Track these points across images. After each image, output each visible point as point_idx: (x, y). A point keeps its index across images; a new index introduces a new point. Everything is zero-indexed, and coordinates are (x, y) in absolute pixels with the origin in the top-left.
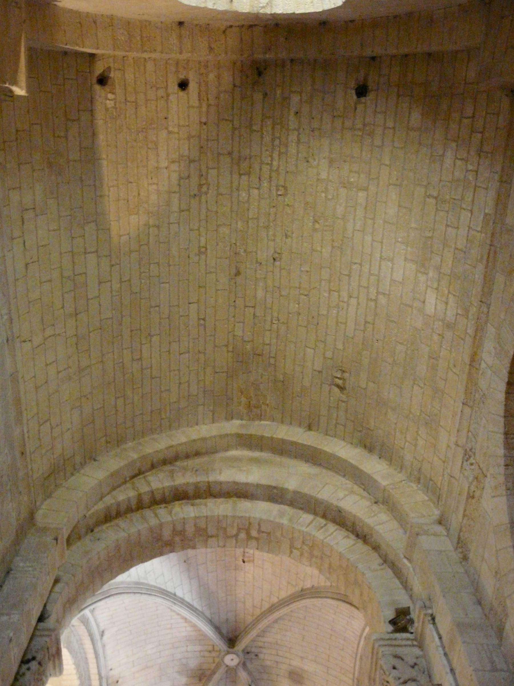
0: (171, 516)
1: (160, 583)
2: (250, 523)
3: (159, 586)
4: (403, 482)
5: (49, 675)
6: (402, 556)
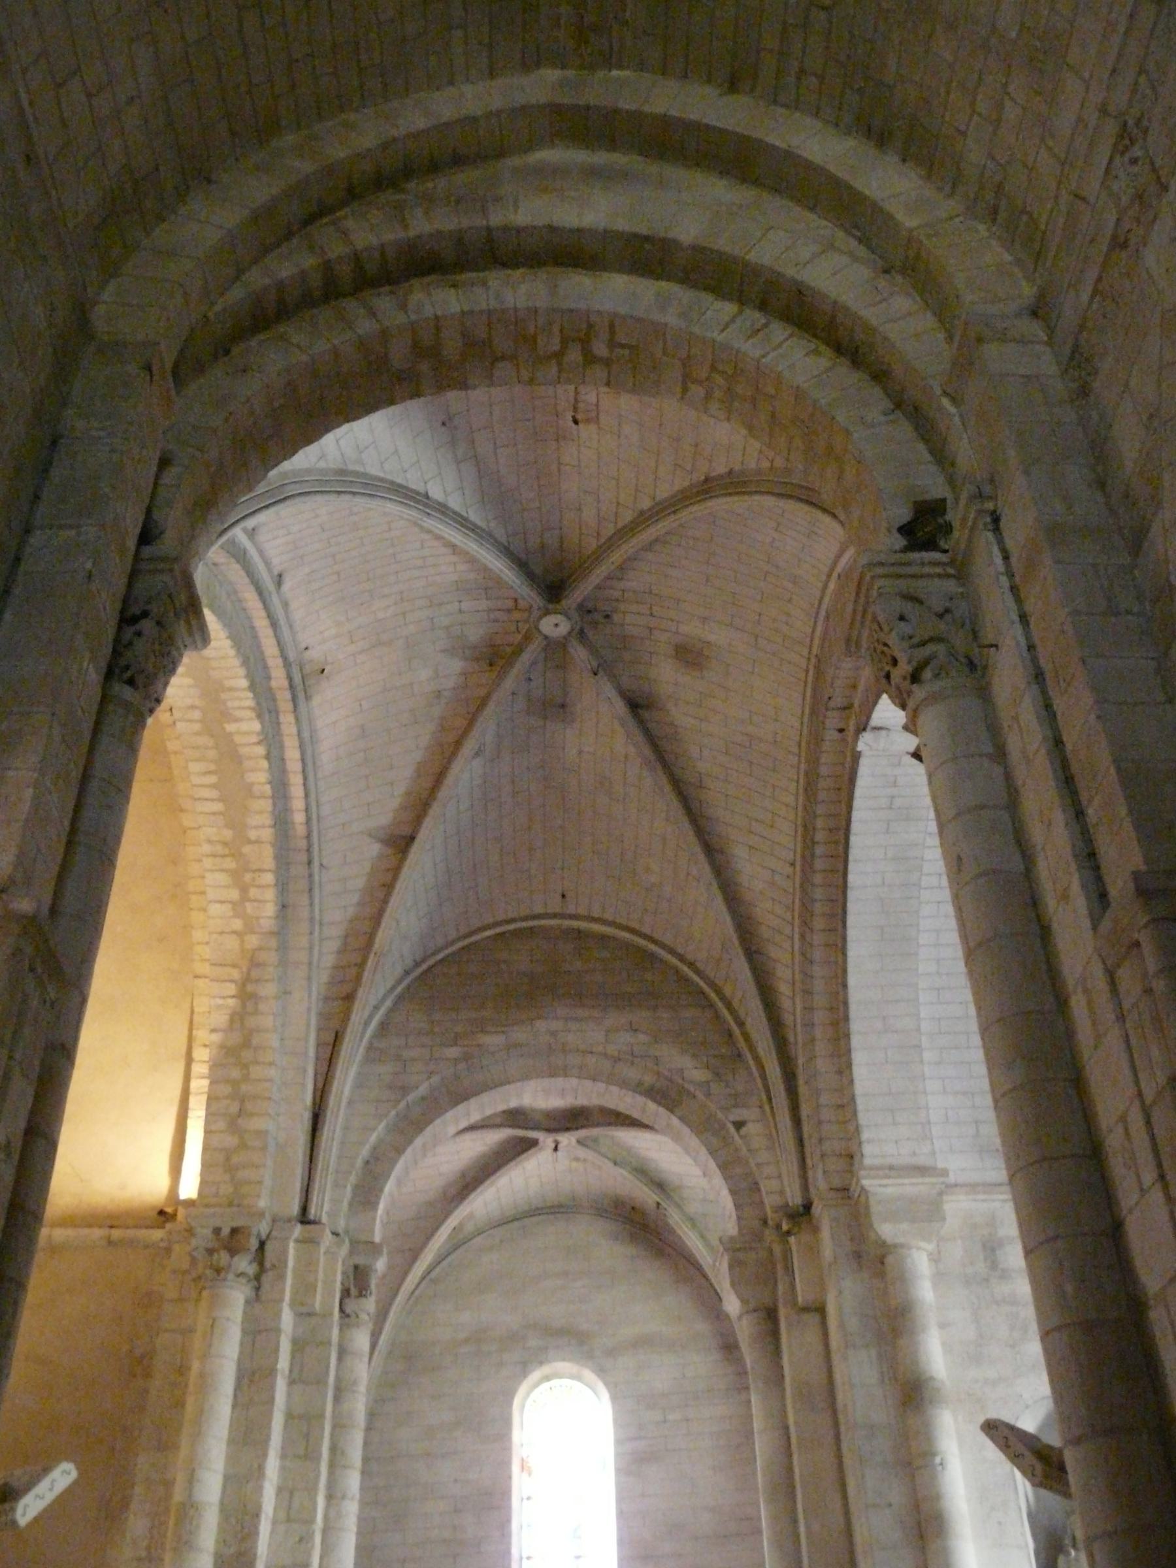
0: (406, 312)
1: (392, 471)
2: (590, 326)
3: (389, 477)
4: (957, 220)
5: (182, 647)
6: (939, 392)
